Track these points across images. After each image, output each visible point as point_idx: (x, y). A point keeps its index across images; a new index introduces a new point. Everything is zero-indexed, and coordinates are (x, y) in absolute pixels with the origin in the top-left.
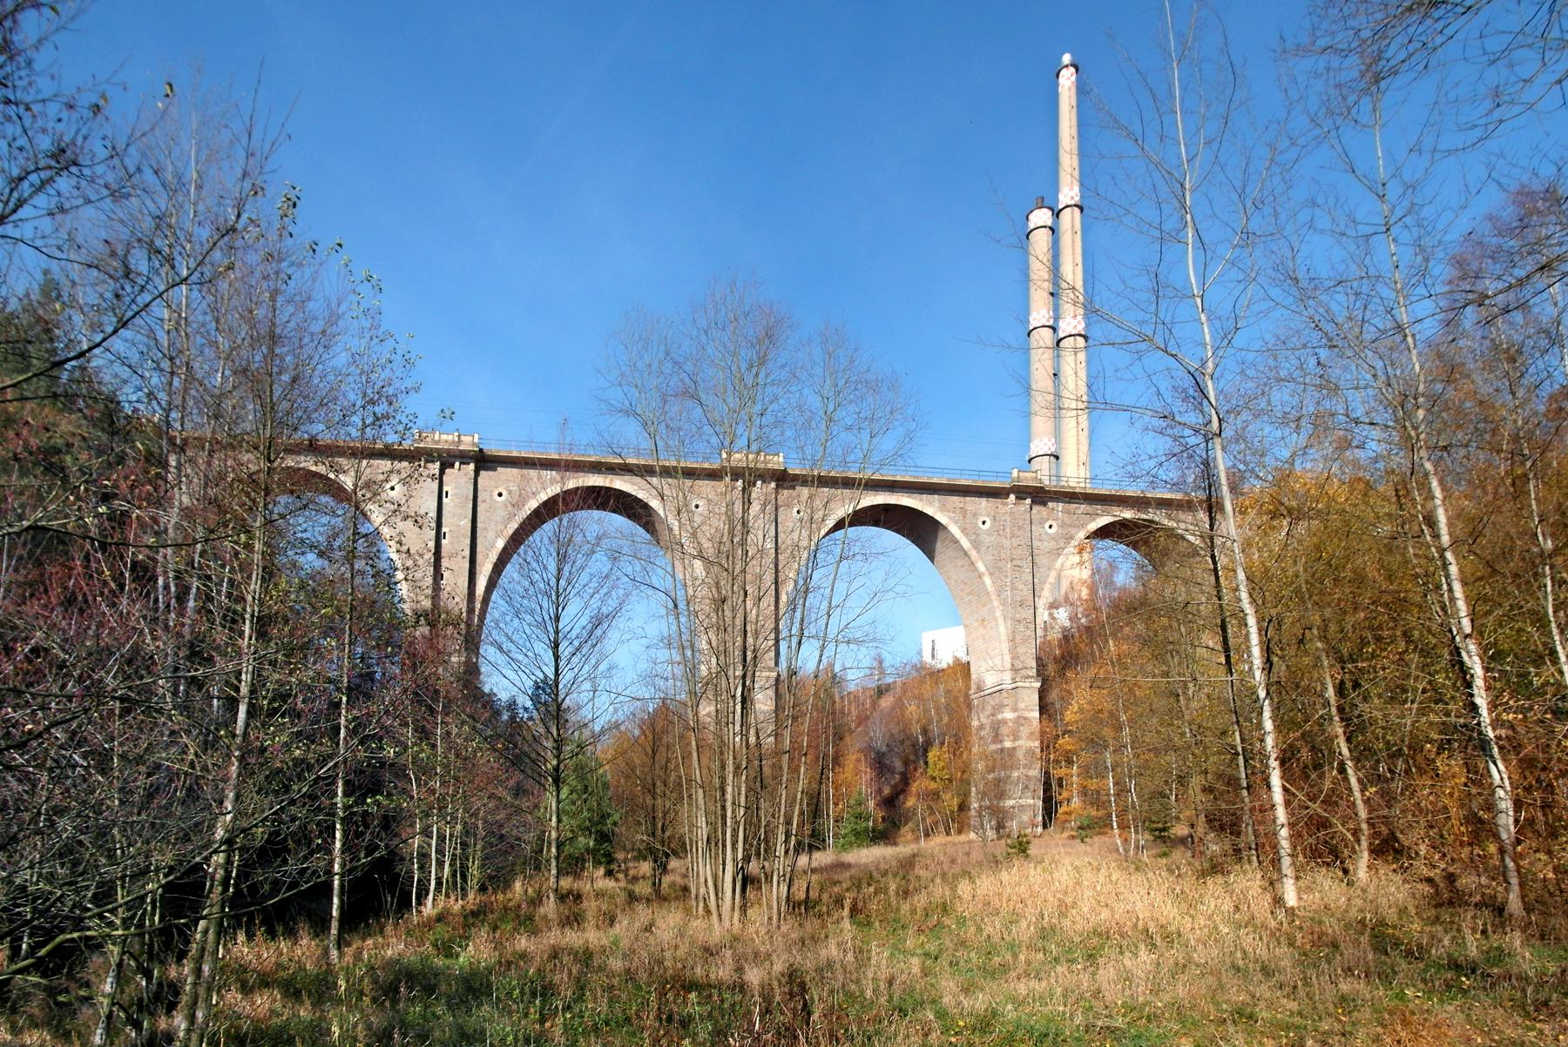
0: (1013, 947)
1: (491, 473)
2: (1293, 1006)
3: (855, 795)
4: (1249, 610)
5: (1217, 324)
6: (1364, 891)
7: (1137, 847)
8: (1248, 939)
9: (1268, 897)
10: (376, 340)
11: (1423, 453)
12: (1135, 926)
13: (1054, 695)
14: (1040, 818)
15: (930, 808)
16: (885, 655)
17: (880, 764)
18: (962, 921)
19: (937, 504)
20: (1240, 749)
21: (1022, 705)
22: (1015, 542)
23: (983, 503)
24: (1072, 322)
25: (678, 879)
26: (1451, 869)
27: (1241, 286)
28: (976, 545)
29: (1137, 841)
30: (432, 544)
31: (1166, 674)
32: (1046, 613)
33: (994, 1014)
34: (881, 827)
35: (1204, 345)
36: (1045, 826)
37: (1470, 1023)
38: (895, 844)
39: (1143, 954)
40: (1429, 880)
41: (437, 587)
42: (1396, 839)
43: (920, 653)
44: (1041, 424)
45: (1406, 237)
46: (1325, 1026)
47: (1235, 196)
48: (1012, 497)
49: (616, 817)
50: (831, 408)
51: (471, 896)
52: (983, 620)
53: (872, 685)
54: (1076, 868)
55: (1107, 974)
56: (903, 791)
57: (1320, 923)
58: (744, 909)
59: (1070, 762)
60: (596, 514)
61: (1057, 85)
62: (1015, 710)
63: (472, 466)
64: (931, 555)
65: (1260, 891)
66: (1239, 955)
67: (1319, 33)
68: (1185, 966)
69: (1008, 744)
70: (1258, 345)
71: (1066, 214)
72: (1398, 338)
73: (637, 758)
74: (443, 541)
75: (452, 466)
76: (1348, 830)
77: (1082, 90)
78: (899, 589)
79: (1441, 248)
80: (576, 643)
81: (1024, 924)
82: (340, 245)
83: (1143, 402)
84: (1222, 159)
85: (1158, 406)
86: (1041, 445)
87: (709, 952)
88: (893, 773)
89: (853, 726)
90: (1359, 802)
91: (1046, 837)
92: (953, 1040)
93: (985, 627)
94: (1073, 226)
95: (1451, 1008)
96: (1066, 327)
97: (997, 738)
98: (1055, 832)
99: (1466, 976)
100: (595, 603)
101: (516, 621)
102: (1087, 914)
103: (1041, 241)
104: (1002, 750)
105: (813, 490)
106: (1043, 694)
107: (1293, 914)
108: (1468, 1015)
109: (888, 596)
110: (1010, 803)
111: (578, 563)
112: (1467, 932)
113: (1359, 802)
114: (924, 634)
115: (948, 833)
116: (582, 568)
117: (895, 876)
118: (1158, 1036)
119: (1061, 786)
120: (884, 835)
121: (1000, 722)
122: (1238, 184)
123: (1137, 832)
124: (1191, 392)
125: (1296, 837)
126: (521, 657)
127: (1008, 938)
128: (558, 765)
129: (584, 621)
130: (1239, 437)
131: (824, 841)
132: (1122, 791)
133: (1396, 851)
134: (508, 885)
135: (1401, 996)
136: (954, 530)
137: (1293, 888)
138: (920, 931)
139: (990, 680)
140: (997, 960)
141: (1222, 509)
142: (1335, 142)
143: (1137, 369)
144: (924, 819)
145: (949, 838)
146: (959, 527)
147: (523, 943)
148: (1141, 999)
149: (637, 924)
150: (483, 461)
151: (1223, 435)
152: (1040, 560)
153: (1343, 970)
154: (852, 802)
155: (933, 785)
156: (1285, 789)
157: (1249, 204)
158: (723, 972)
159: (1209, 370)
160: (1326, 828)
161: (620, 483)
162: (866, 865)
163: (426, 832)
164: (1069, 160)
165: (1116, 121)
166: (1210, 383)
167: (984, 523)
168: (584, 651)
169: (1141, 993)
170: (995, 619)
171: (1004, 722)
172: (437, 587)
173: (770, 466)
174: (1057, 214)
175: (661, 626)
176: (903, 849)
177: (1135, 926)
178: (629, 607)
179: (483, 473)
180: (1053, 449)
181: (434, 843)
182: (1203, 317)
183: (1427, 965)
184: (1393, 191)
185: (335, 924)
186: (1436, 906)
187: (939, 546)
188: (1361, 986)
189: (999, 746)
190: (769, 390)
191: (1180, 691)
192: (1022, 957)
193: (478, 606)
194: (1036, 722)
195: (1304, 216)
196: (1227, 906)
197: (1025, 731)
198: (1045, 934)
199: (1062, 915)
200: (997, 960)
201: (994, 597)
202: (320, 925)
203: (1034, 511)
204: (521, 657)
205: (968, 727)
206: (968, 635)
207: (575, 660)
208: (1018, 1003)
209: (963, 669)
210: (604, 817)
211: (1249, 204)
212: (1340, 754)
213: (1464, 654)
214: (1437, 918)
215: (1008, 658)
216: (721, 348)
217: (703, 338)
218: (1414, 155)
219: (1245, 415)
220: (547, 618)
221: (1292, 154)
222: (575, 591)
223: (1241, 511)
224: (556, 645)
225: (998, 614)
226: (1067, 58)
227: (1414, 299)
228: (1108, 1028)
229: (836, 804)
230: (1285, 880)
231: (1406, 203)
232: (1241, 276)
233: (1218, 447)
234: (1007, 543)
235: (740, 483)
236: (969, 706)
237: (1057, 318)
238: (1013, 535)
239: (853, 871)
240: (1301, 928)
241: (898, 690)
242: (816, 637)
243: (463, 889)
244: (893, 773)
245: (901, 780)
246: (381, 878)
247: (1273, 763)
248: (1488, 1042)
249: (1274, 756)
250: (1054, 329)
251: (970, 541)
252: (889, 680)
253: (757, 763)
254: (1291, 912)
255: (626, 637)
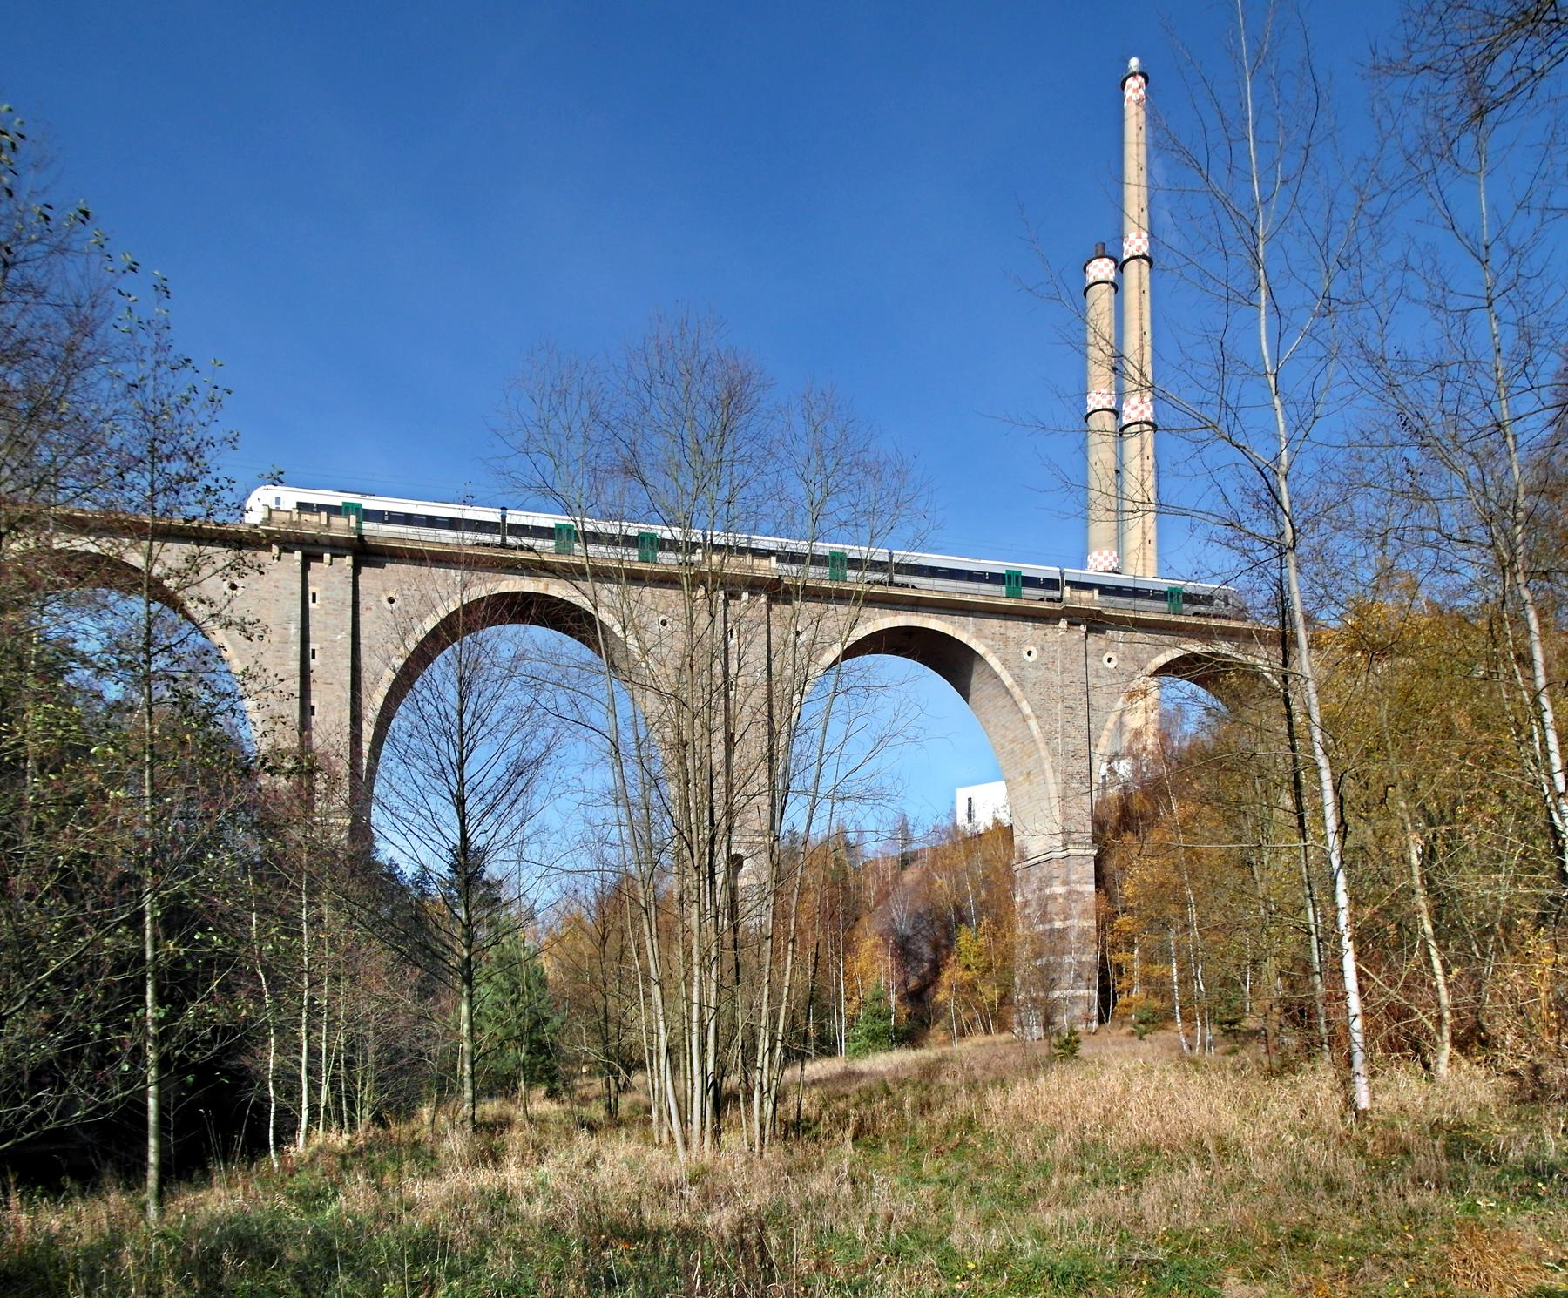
0: (1045, 1169)
1: (377, 570)
2: (1354, 1224)
3: (872, 988)
4: (1323, 762)
5: (1292, 410)
6: (1445, 1088)
7: (1203, 1044)
8: (1314, 1150)
9: (1339, 1098)
10: (164, 367)
11: (1520, 578)
12: (1189, 1137)
13: (1112, 864)
14: (1096, 1012)
15: (965, 1001)
16: (912, 813)
17: (903, 950)
18: (988, 1139)
19: (972, 628)
20: (1313, 928)
21: (1074, 877)
22: (1068, 678)
23: (1028, 629)
24: (1138, 407)
25: (642, 1097)
26: (1537, 1061)
27: (1323, 363)
28: (1020, 681)
29: (1203, 1036)
30: (295, 666)
31: (1238, 839)
32: (1105, 767)
33: (1012, 1252)
34: (904, 1027)
35: (1276, 436)
36: (1101, 1021)
37: (1543, 1234)
38: (922, 1046)
39: (1196, 1172)
40: (1514, 1074)
41: (304, 725)
42: (1482, 1029)
43: (953, 813)
44: (1101, 530)
45: (1510, 314)
46: (1388, 1246)
47: (1315, 249)
48: (1063, 624)
49: (556, 1022)
50: (818, 496)
51: (361, 1128)
52: (1029, 774)
53: (895, 852)
54: (1126, 1072)
55: (1151, 1196)
56: (932, 982)
57: (1393, 1127)
58: (717, 1133)
59: (1130, 944)
60: (511, 629)
61: (1123, 97)
62: (1066, 883)
63: (349, 560)
64: (964, 692)
65: (1329, 1091)
66: (1303, 1168)
67: (1415, 47)
68: (1242, 1183)
69: (1058, 924)
70: (1340, 440)
71: (1132, 267)
72: (1497, 437)
73: (586, 946)
74: (312, 662)
75: (320, 558)
76: (1430, 1019)
77: (1151, 104)
78: (911, 732)
79: (1547, 331)
80: (490, 798)
81: (1059, 1140)
82: (86, 213)
83: (1203, 506)
84: (1300, 203)
85: (1222, 508)
86: (1100, 559)
87: (665, 1189)
88: (921, 961)
89: (872, 904)
90: (1442, 987)
91: (1103, 1033)
92: (958, 1286)
93: (1031, 782)
94: (1140, 284)
95: (1525, 1218)
96: (1130, 413)
97: (1045, 917)
98: (1113, 1027)
99: (1543, 1181)
100: (514, 745)
101: (402, 768)
102: (1137, 1125)
103: (1101, 299)
104: (1051, 930)
105: (854, 609)
106: (1099, 862)
107: (1365, 1118)
108: (1541, 1226)
109: (895, 741)
110: (1057, 994)
111: (488, 694)
112: (1547, 1132)
113: (1442, 987)
114: (959, 791)
115: (987, 1032)
116: (495, 698)
117: (915, 1088)
118: (1203, 1268)
119: (1121, 974)
120: (909, 1036)
121: (1048, 897)
122: (1320, 234)
123: (1203, 1025)
124: (1264, 495)
125: (1370, 1032)
126: (411, 816)
127: (1040, 1158)
128: (469, 958)
129: (499, 769)
130: (1318, 554)
131: (835, 1045)
132: (1185, 981)
133: (1483, 1043)
134: (410, 1115)
135: (1472, 1208)
136: (993, 661)
137: (1365, 1087)
138: (939, 1152)
139: (1035, 847)
140: (1026, 1184)
141: (1296, 643)
142: (1432, 187)
143: (1196, 463)
144: (958, 1016)
145: (989, 1038)
146: (1000, 658)
147: (417, 1188)
148: (1188, 1225)
149: (576, 1158)
150: (365, 554)
151: (1298, 551)
152: (1098, 700)
153: (1413, 1181)
154: (869, 996)
155: (968, 976)
156: (1360, 973)
157: (1333, 262)
158: (669, 1217)
159: (1283, 469)
160: (1407, 1017)
161: (558, 589)
162: (881, 1074)
163: (288, 1046)
164: (1135, 198)
165: (1175, 142)
166: (1283, 485)
167: (1029, 653)
168: (501, 808)
169: (1189, 1216)
170: (1043, 772)
171: (1054, 897)
172: (304, 725)
173: (759, 574)
174: (1120, 266)
175: (603, 778)
176: (928, 1053)
177: (1189, 1137)
178: (562, 752)
179: (364, 569)
180: (1115, 565)
181: (304, 1060)
182: (1277, 401)
183: (1503, 1171)
184: (1498, 255)
185: (152, 1173)
186: (1518, 1103)
187: (975, 681)
188: (1430, 1197)
189: (1048, 927)
190: (738, 469)
191: (1254, 860)
192: (1055, 1182)
193: (366, 747)
194: (1093, 898)
195: (1394, 283)
196: (1293, 1111)
197: (1077, 908)
198: (1083, 1151)
199: (1107, 1127)
200: (1026, 1184)
201: (1042, 745)
202: (132, 1175)
203: (1089, 641)
204: (411, 816)
205: (1010, 900)
206: (1010, 792)
207: (489, 819)
208: (1040, 1237)
209: (1005, 833)
210: (539, 1022)
211: (1333, 262)
212: (1424, 933)
213: (1555, 816)
214: (1519, 1116)
215: (1058, 819)
216: (670, 410)
217: (644, 393)
218: (1522, 213)
219: (1324, 527)
220: (446, 763)
221: (1380, 202)
222: (485, 730)
223: (1315, 644)
224: (460, 802)
225: (1047, 766)
226: (1134, 63)
227: (1514, 391)
228: (1146, 1261)
229: (849, 1000)
230: (1357, 1079)
231: (1511, 272)
232: (1322, 353)
233: (1292, 562)
234: (1057, 679)
235: (701, 592)
236: (1013, 880)
237: (1120, 402)
238: (1064, 670)
239: (864, 1082)
240: (1372, 1133)
241: (928, 859)
242: (805, 792)
243: (352, 1121)
244: (921, 961)
245: (931, 970)
246: (207, 1112)
247: (1347, 944)
248: (1560, 1255)
249: (1347, 935)
250: (1117, 413)
251: (1012, 675)
252: (916, 847)
253: (729, 954)
254: (1362, 1115)
255: (557, 790)
